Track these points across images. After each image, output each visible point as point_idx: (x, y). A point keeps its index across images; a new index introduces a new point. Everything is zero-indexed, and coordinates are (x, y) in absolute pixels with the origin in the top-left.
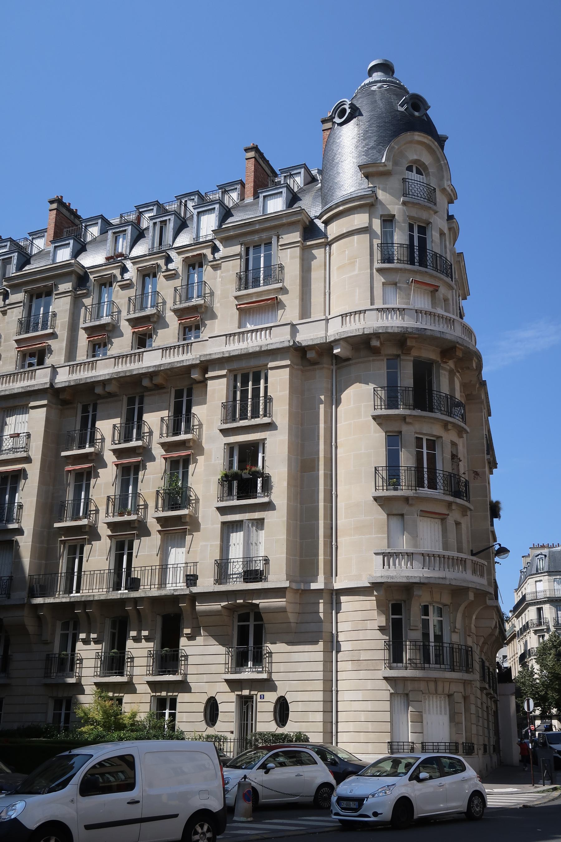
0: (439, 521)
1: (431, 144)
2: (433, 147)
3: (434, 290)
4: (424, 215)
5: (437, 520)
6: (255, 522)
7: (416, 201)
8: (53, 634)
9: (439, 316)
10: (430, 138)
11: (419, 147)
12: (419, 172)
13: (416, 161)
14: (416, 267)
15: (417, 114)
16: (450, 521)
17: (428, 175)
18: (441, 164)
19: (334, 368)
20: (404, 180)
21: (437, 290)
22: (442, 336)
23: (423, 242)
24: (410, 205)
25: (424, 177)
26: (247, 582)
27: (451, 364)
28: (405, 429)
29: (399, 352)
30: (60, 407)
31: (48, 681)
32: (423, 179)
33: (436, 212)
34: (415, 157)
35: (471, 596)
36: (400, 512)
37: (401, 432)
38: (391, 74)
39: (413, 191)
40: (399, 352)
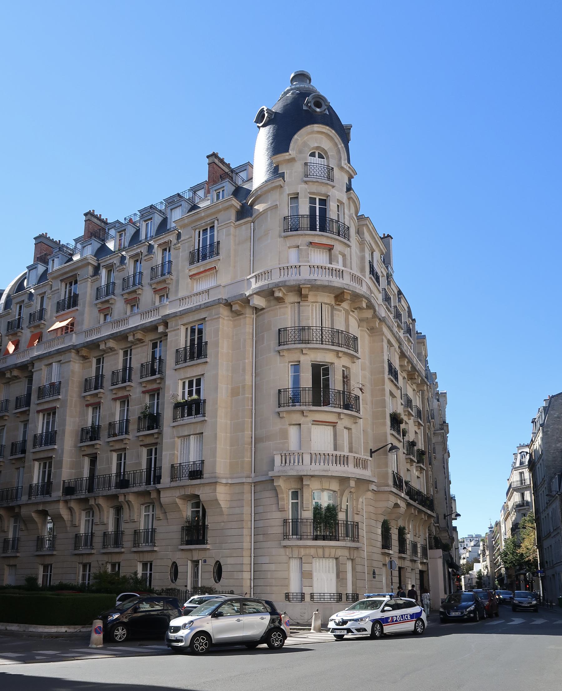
0: (332, 428)
1: (329, 132)
2: (331, 134)
3: (330, 248)
4: (323, 190)
5: (329, 427)
6: (198, 436)
7: (314, 180)
8: (80, 520)
10: (328, 128)
11: (319, 136)
12: (321, 156)
13: (318, 148)
14: (318, 232)
15: (318, 110)
16: (340, 426)
17: (328, 158)
18: (338, 148)
19: (254, 316)
20: (306, 164)
22: (330, 284)
23: (323, 212)
24: (311, 183)
28: (302, 358)
30: (82, 362)
32: (324, 161)
33: (333, 187)
34: (316, 145)
35: (352, 483)
37: (300, 361)
38: (308, 81)
39: (320, 173)
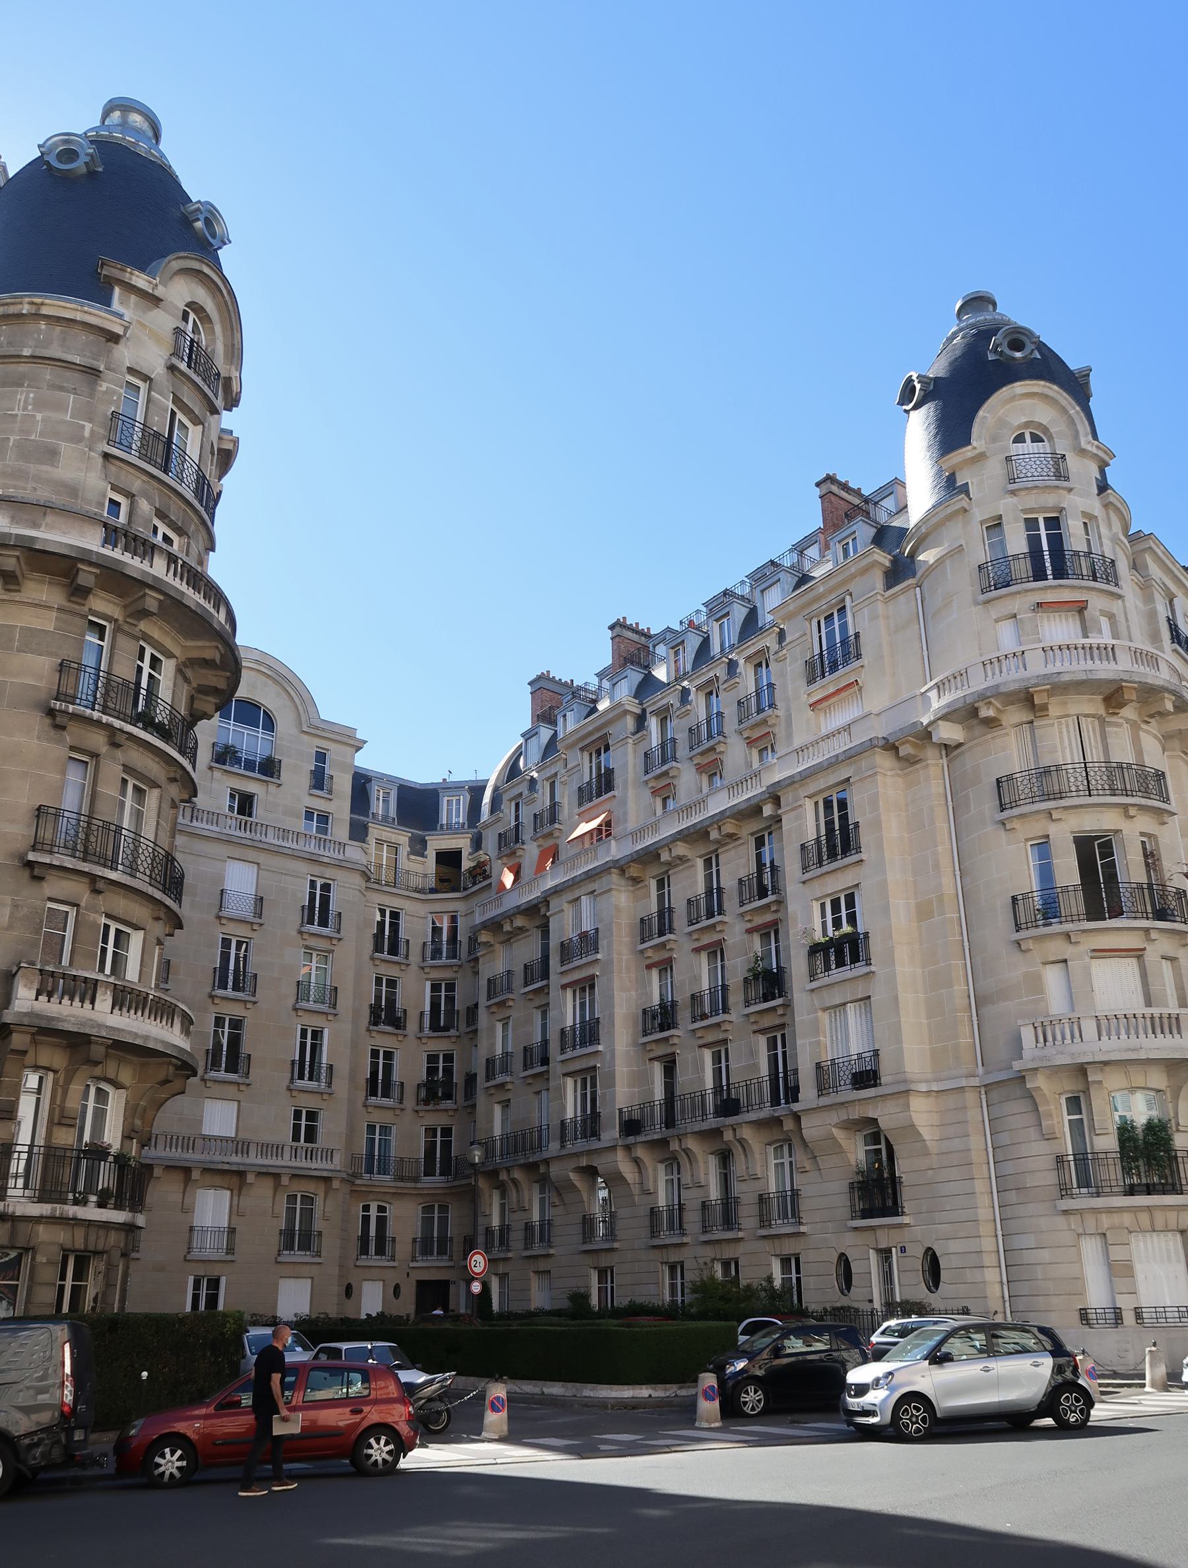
0: (1134, 960)
1: (1046, 391)
2: (1051, 393)
4: (1050, 500)
6: (862, 1003)
9: (1083, 648)
10: (1042, 383)
12: (1036, 439)
15: (1018, 355)
17: (1051, 438)
19: (945, 761)
20: (1008, 459)
21: (1086, 608)
22: (1090, 677)
24: (1023, 493)
25: (1046, 443)
26: (857, 1089)
27: (1128, 712)
28: (1053, 829)
29: (1031, 717)
31: (656, 1242)
36: (1060, 958)
37: (1048, 836)
38: (991, 307)
40: (1031, 717)
